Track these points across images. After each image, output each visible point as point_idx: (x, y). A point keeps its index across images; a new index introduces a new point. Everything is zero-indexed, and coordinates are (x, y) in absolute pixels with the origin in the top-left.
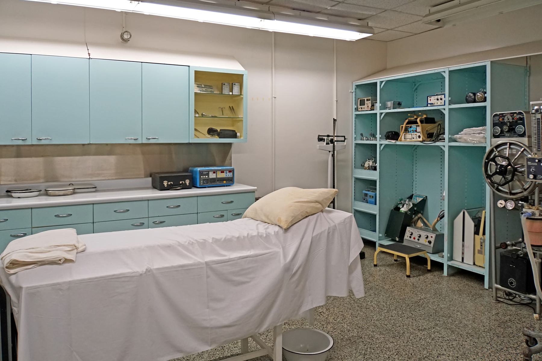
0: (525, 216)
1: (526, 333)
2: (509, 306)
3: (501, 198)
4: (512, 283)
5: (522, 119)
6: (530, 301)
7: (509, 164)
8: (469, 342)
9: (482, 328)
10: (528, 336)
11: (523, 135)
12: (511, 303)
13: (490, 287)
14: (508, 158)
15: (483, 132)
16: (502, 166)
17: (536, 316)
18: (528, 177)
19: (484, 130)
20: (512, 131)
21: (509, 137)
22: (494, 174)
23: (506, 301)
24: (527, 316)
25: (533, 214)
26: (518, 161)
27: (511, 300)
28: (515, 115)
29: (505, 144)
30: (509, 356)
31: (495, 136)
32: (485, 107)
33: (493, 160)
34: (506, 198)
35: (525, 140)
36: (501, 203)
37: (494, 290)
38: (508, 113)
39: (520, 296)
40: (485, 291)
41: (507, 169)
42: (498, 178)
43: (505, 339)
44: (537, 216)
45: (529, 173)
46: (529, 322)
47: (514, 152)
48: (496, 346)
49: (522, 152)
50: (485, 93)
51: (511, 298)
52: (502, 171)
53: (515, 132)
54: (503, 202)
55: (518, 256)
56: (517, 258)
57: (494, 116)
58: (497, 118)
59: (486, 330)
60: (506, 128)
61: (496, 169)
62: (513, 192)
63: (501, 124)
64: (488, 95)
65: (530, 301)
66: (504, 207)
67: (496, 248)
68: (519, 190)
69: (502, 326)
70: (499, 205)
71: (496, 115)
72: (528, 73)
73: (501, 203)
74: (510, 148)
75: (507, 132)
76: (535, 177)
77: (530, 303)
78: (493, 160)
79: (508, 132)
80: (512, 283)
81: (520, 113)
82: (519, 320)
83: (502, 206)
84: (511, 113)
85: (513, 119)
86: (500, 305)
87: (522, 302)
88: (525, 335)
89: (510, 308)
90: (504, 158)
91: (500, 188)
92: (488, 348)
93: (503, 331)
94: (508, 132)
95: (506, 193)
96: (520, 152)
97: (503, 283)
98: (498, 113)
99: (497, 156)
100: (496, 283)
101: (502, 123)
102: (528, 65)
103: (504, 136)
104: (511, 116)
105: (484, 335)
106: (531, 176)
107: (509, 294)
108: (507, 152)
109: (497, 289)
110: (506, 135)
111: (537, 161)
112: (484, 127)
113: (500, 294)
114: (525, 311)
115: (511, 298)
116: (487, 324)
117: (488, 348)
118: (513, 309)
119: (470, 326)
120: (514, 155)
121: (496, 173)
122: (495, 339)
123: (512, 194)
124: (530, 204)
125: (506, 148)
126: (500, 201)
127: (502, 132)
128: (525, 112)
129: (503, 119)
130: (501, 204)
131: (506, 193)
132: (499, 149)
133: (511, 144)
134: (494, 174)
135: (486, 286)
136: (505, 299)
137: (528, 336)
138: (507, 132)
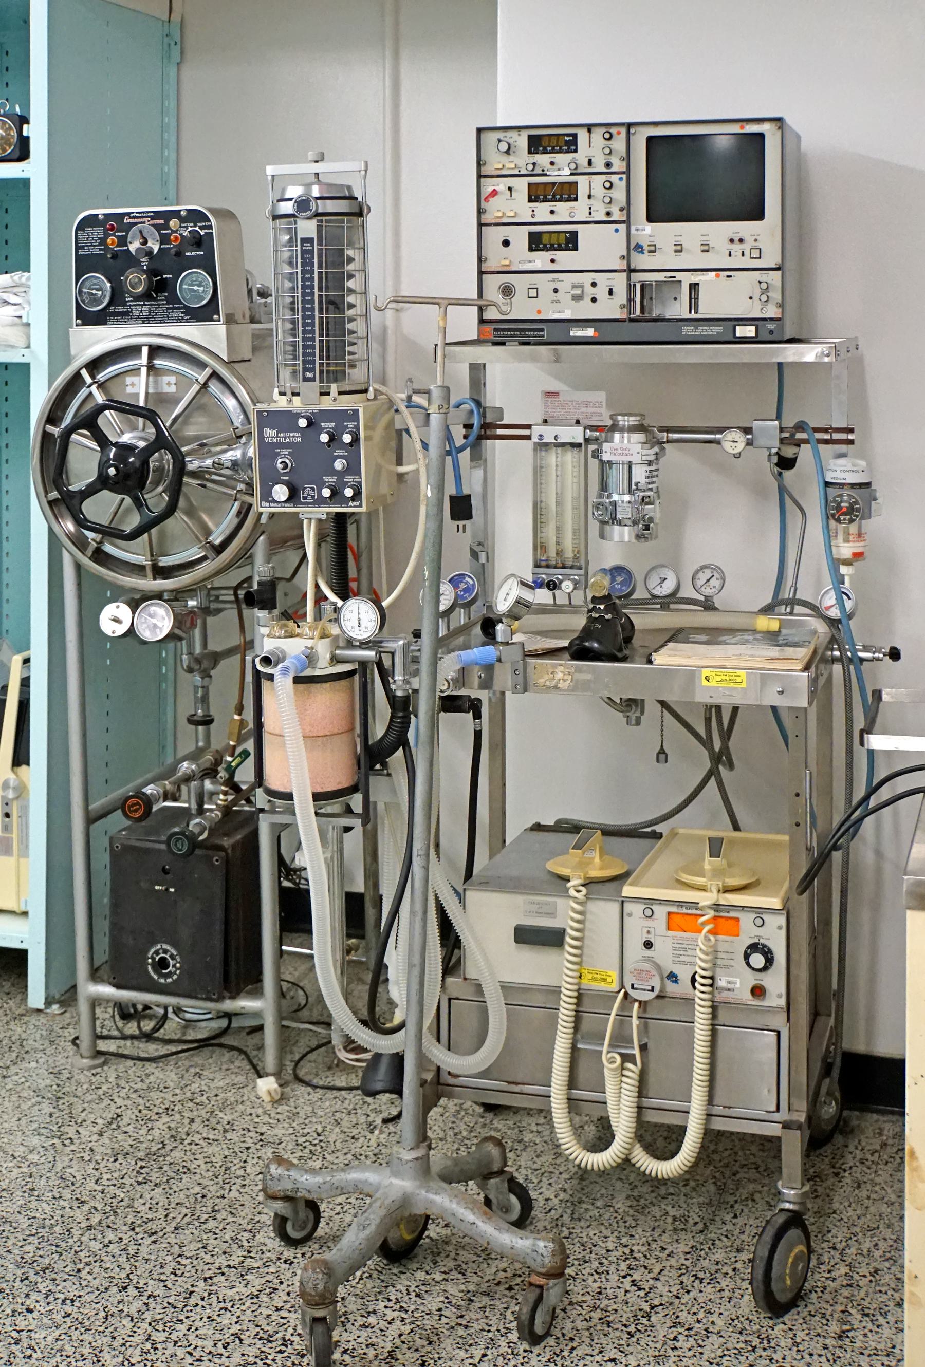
0: (286, 670)
1: (277, 1188)
2: (150, 1067)
3: (118, 594)
4: (162, 964)
5: (201, 242)
6: (224, 1023)
7: (160, 442)
8: (42, 1308)
9: (79, 1215)
10: (287, 1199)
11: (205, 313)
12: (152, 1049)
13: (65, 997)
14: (150, 415)
15: (13, 299)
16: (126, 449)
17: (267, 1085)
18: (267, 496)
19: (24, 289)
20: (160, 292)
21: (147, 321)
22: (90, 491)
23: (128, 1047)
24: (231, 1096)
25: (311, 658)
26: (185, 423)
27: (148, 1037)
28: (174, 223)
29: (131, 351)
30: (226, 1319)
31: (88, 318)
32: (25, 184)
33: (89, 422)
34: (134, 590)
35: (212, 336)
36: (114, 619)
37: (83, 1007)
38: (142, 215)
39: (178, 1011)
40: (33, 1020)
41: (146, 463)
42: (103, 507)
43: (185, 1236)
44: (324, 667)
45: (270, 479)
46: (245, 1123)
47: (168, 385)
48: (160, 1291)
49: (205, 386)
50: (24, 120)
51: (147, 1026)
52: (127, 474)
53: (174, 300)
54: (123, 611)
55: (192, 840)
56: (191, 852)
57: (82, 226)
58: (98, 232)
59: (95, 1219)
60: (136, 281)
61: (103, 465)
62: (164, 562)
63: (115, 263)
64: (37, 131)
65: (224, 1023)
66: (131, 632)
67: (91, 819)
68: (195, 553)
69: (155, 1176)
70: (108, 627)
71: (89, 222)
72: (176, 51)
73: (114, 619)
74: (151, 368)
75: (137, 298)
76: (293, 496)
77: (224, 1032)
78: (89, 422)
79: (146, 296)
80: (162, 964)
81: (196, 216)
82: (206, 1122)
83: (121, 630)
84: (157, 215)
85: (164, 239)
86: (110, 1072)
87: (191, 1035)
88: (274, 1198)
89: (156, 1073)
90: (127, 409)
91: (108, 548)
92: (133, 1311)
93: (163, 1201)
94: (146, 296)
95: (139, 570)
96: (196, 388)
97: (121, 966)
98: (100, 212)
99: (102, 409)
100: (95, 975)
101: (115, 256)
102: (176, 17)
103: (126, 317)
104: (158, 227)
105: (95, 1246)
106: (280, 492)
107: (126, 1013)
108: (138, 388)
109: (95, 1002)
110: (136, 311)
111: (303, 423)
112: (17, 276)
113: (107, 1018)
114: (216, 1076)
115: (147, 1026)
116: (91, 1185)
117: (133, 1311)
118: (167, 1075)
119: (24, 1223)
120: (170, 400)
121: (102, 482)
122: (144, 1251)
123: (161, 572)
124: (286, 615)
125: (136, 371)
126: (110, 611)
127: (117, 296)
128: (210, 210)
129: (123, 241)
130: (116, 620)
131: (139, 570)
132: (101, 376)
133: (155, 351)
134: (90, 491)
135: (36, 994)
136: (124, 1037)
137: (287, 1199)
138: (137, 298)
